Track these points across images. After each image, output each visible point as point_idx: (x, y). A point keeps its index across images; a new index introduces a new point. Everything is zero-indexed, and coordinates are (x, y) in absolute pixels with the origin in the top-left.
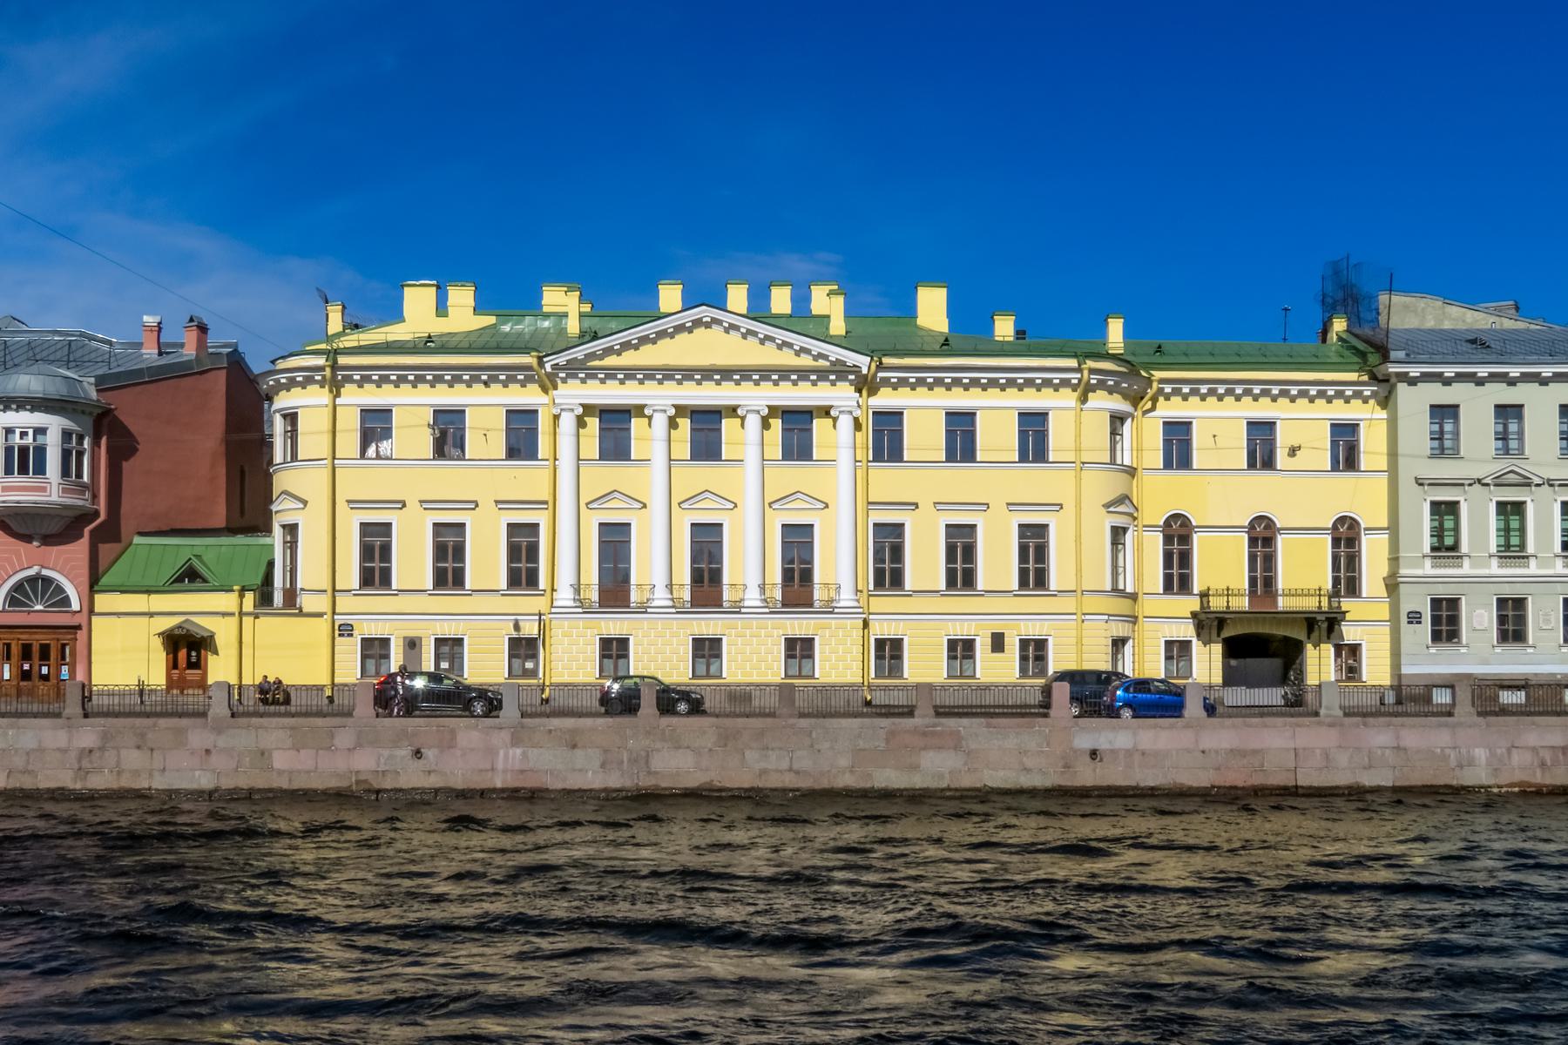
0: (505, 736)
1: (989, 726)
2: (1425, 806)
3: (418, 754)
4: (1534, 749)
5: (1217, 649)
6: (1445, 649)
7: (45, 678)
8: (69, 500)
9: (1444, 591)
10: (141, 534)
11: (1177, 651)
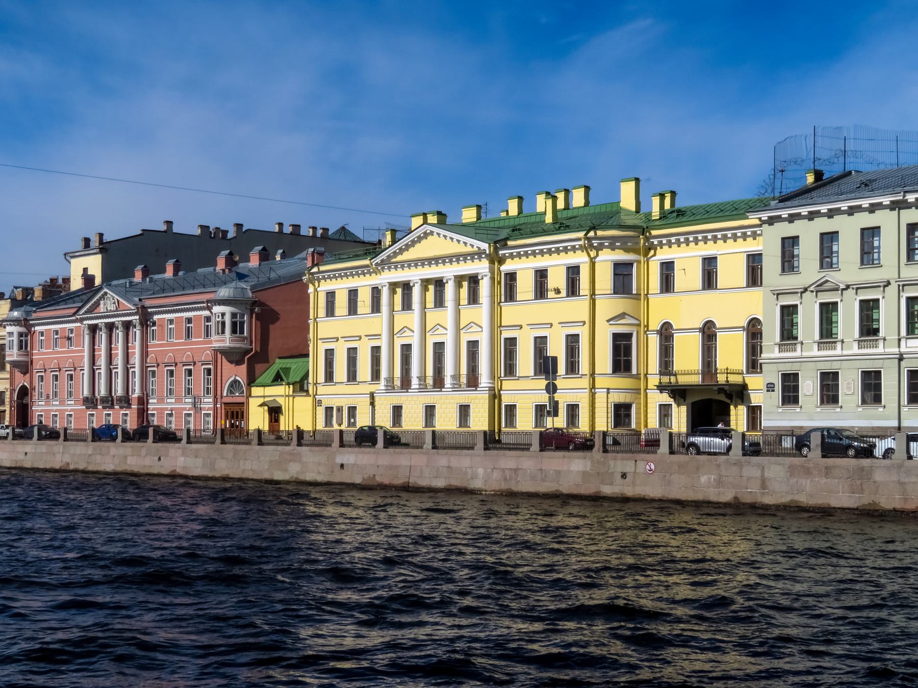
0: (180, 451)
1: (311, 451)
2: (724, 515)
3: (160, 459)
4: (503, 470)
5: (684, 409)
6: (791, 409)
7: (237, 426)
8: (232, 345)
9: (789, 369)
10: (280, 358)
11: (665, 411)
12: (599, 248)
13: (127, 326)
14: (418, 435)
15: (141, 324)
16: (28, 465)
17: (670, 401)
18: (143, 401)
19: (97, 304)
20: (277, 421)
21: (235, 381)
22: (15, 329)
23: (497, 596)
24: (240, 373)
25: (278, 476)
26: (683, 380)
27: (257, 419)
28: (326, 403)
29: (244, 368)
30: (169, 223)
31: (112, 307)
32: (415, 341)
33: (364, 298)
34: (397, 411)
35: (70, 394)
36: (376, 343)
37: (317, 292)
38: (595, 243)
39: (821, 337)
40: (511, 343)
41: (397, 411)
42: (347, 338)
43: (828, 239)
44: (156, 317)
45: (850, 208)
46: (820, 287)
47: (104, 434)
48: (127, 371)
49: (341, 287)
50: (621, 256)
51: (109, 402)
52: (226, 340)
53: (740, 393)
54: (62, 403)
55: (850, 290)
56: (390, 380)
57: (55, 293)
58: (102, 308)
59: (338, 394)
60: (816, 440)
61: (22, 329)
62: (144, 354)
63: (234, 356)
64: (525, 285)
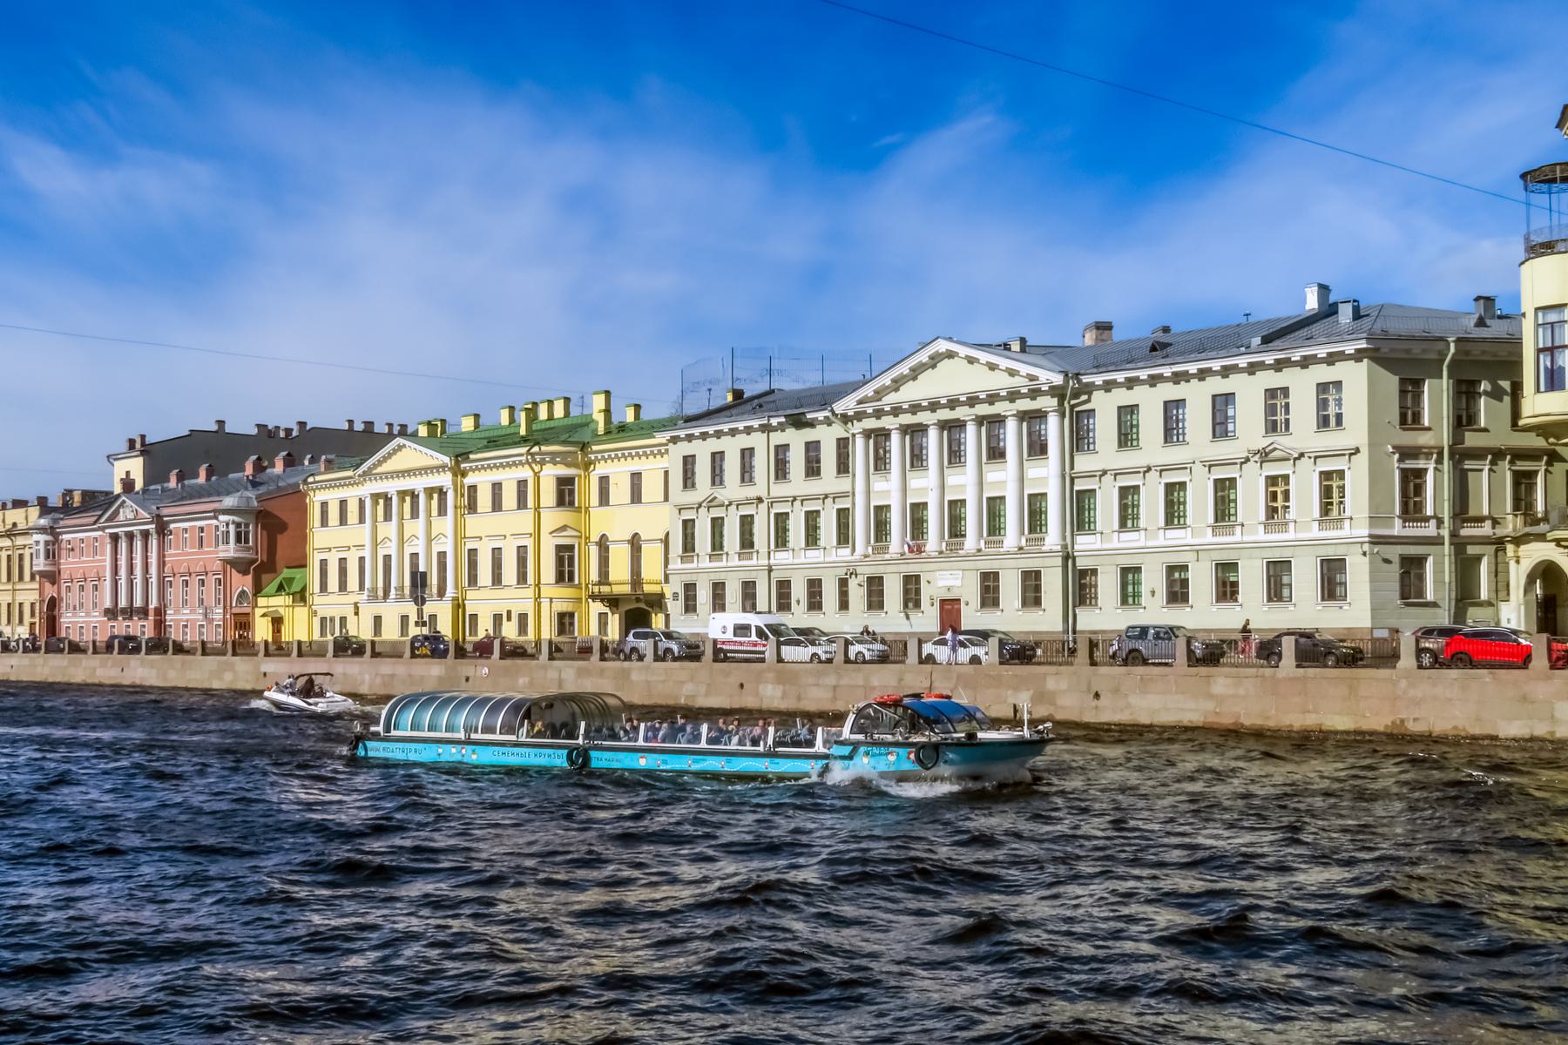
12: (542, 463)
13: (146, 535)
14: (394, 644)
15: (158, 533)
16: (13, 678)
17: (607, 610)
18: (160, 612)
19: (116, 513)
20: (279, 631)
21: (243, 592)
22: (42, 538)
23: (799, 837)
24: (243, 583)
25: (216, 685)
26: (617, 590)
27: (262, 631)
28: (321, 614)
29: (249, 578)
30: (221, 423)
31: (131, 516)
32: (448, 548)
33: (353, 508)
34: (378, 620)
35: (95, 605)
36: (361, 554)
37: (316, 498)
38: (538, 458)
39: (1216, 520)
40: (473, 553)
41: (378, 620)
42: (339, 548)
43: (1172, 409)
44: (172, 526)
45: (1330, 354)
46: (711, 503)
47: (128, 645)
48: (146, 581)
49: (333, 496)
50: (563, 471)
51: (130, 612)
52: (230, 550)
53: (657, 602)
54: (193, 612)
55: (1304, 460)
56: (374, 589)
57: (96, 502)
58: (121, 517)
59: (331, 604)
60: (1288, 645)
61: (49, 538)
62: (162, 563)
63: (240, 566)
64: (484, 499)
